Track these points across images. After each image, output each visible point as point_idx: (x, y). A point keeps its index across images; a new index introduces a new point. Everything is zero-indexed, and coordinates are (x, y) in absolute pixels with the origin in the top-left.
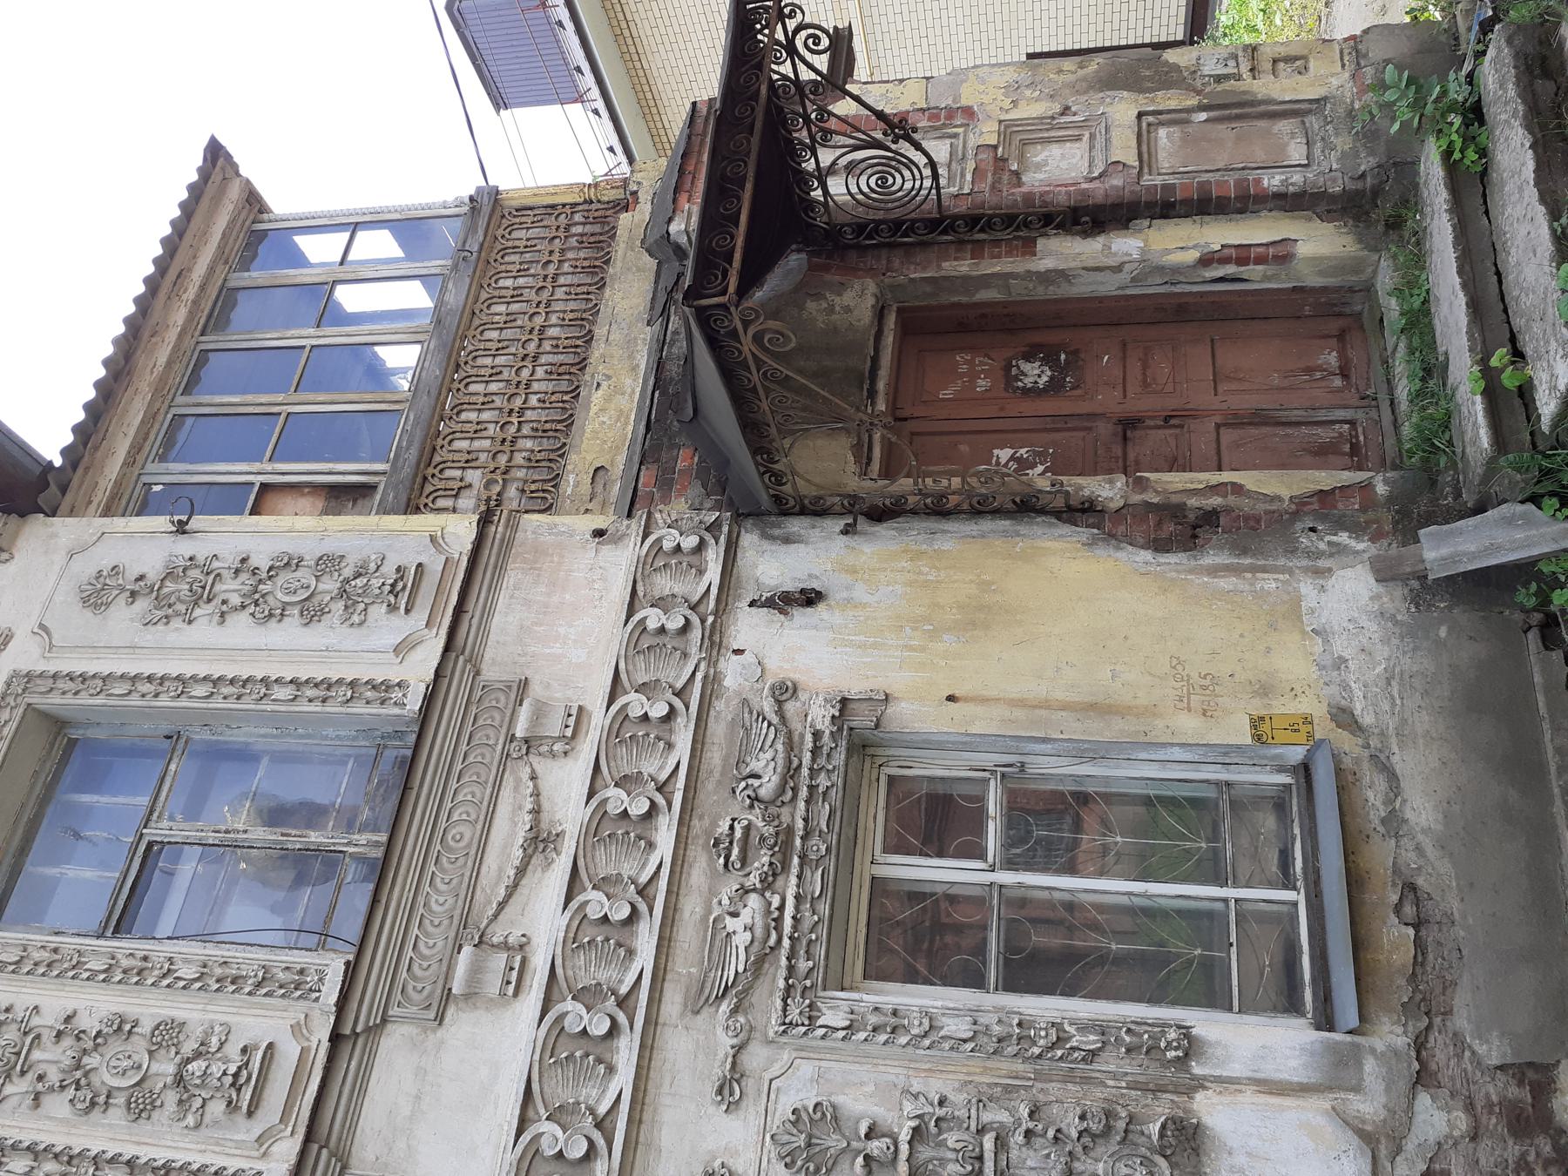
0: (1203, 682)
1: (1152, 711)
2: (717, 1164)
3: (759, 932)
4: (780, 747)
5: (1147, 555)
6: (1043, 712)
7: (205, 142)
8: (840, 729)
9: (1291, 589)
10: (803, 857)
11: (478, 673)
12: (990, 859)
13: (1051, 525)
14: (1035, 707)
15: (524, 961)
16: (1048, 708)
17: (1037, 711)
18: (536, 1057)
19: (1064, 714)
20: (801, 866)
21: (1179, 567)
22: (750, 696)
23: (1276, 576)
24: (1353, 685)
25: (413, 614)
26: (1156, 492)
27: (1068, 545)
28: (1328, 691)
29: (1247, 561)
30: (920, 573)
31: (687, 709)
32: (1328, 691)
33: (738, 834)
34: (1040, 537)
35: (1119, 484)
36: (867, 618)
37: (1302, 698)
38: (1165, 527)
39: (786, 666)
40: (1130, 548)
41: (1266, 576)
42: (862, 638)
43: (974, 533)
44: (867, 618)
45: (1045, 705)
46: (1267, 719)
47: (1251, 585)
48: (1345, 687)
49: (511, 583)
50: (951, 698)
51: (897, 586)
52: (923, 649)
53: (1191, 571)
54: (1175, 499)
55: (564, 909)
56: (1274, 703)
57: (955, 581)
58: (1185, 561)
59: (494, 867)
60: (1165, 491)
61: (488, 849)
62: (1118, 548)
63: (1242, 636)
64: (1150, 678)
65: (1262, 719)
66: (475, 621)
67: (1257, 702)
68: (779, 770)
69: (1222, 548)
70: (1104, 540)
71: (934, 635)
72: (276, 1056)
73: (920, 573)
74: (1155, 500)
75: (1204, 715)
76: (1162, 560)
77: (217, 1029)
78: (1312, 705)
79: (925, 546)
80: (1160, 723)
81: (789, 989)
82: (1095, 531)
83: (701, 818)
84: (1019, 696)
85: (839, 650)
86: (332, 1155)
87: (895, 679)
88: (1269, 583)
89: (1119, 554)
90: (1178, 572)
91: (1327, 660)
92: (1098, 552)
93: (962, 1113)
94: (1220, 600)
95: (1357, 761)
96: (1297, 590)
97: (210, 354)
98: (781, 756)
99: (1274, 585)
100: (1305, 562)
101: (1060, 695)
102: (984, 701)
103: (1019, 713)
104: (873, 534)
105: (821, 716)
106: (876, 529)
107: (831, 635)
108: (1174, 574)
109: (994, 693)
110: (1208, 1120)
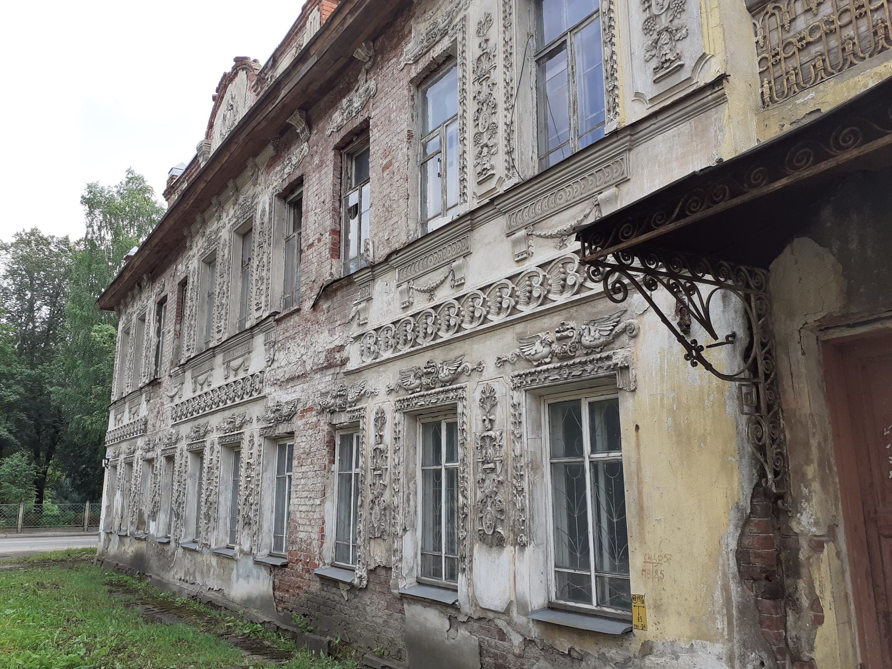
0: (659, 572)
1: (643, 541)
2: (484, 365)
3: (537, 356)
4: (602, 340)
5: (733, 545)
6: (636, 480)
8: (613, 369)
9: (718, 637)
10: (560, 368)
11: (630, 150)
12: (593, 456)
13: (751, 480)
14: (638, 476)
15: (526, 258)
16: (638, 483)
17: (636, 476)
18: (498, 283)
19: (636, 492)
20: (558, 368)
21: (726, 566)
22: (629, 312)
23: (726, 629)
24: (664, 659)
25: (658, 85)
26: (809, 558)
27: (736, 492)
28: (660, 644)
29: (735, 612)
30: (709, 395)
31: (481, 324)
32: (660, 644)
33: (565, 334)
34: (741, 472)
35: (814, 529)
36: (678, 368)
37: (654, 628)
38: (759, 560)
39: (646, 327)
40: (738, 534)
41: (726, 623)
42: (666, 367)
43: (740, 427)
44: (678, 368)
45: (640, 482)
46: (643, 605)
47: (719, 612)
48: (662, 655)
49: (682, 129)
50: (637, 427)
51: (699, 381)
52: (662, 406)
53: (724, 574)
54: (804, 571)
55: (507, 278)
56: (651, 611)
57: (705, 419)
58: (731, 571)
59: (553, 222)
60: (810, 565)
61: (559, 215)
62: (736, 526)
63: (686, 599)
64: (659, 542)
65: (643, 602)
66: (653, 127)
67: (651, 601)
68: (591, 343)
69: (742, 597)
70: (742, 516)
71: (671, 412)
72: (681, 72)
73: (709, 395)
74: (801, 556)
75: (643, 570)
76: (730, 555)
77: (684, 31)
78: (651, 633)
79: (727, 394)
80: (637, 545)
81: (520, 376)
82: (749, 511)
83: (577, 311)
84: (642, 466)
85: (658, 355)
86: (471, 224)
87: (643, 394)
88: (721, 624)
89: (732, 528)
90: (723, 565)
91: (677, 649)
92: (732, 512)
93: (498, 455)
94: (706, 589)
95: (627, 649)
96: (718, 641)
98: (597, 342)
99: (719, 627)
100: (737, 652)
101: (646, 490)
102: (638, 446)
103: (634, 467)
104: (735, 356)
105: (619, 357)
106: (738, 357)
107: (666, 348)
108: (721, 562)
109: (642, 452)
110: (505, 550)
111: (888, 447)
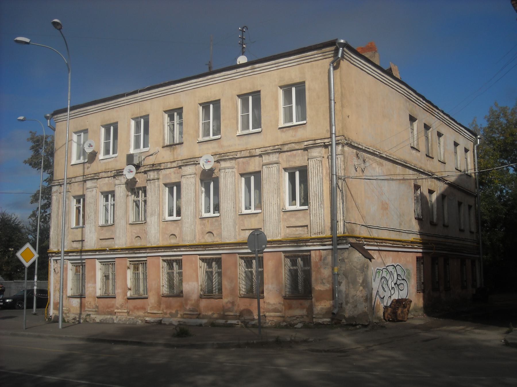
97: (328, 149)
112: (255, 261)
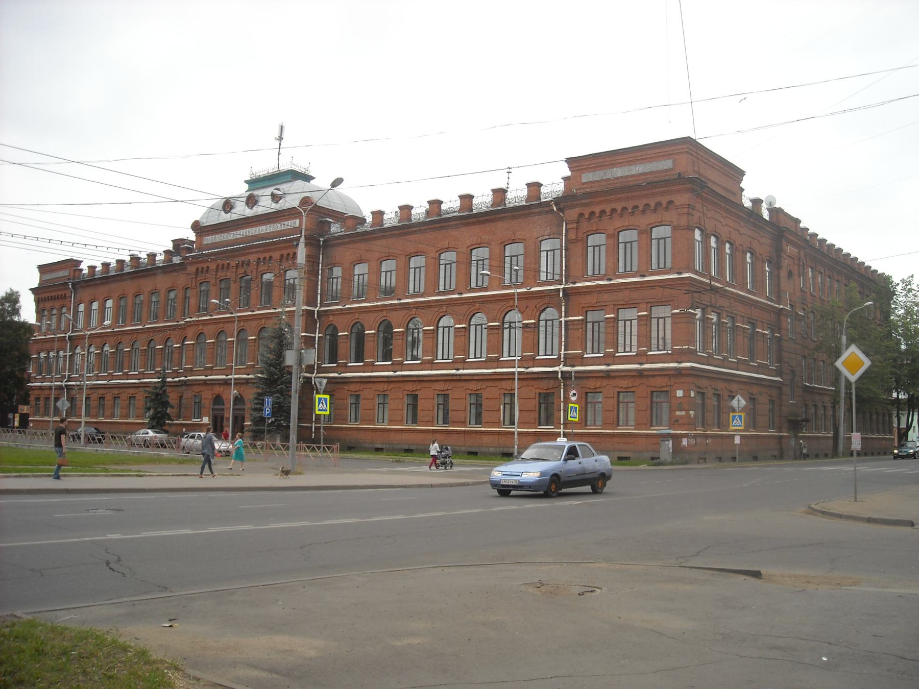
7: (472, 193)
111: (824, 659)
112: (735, 443)
